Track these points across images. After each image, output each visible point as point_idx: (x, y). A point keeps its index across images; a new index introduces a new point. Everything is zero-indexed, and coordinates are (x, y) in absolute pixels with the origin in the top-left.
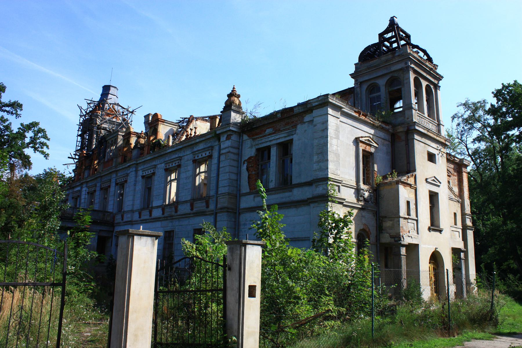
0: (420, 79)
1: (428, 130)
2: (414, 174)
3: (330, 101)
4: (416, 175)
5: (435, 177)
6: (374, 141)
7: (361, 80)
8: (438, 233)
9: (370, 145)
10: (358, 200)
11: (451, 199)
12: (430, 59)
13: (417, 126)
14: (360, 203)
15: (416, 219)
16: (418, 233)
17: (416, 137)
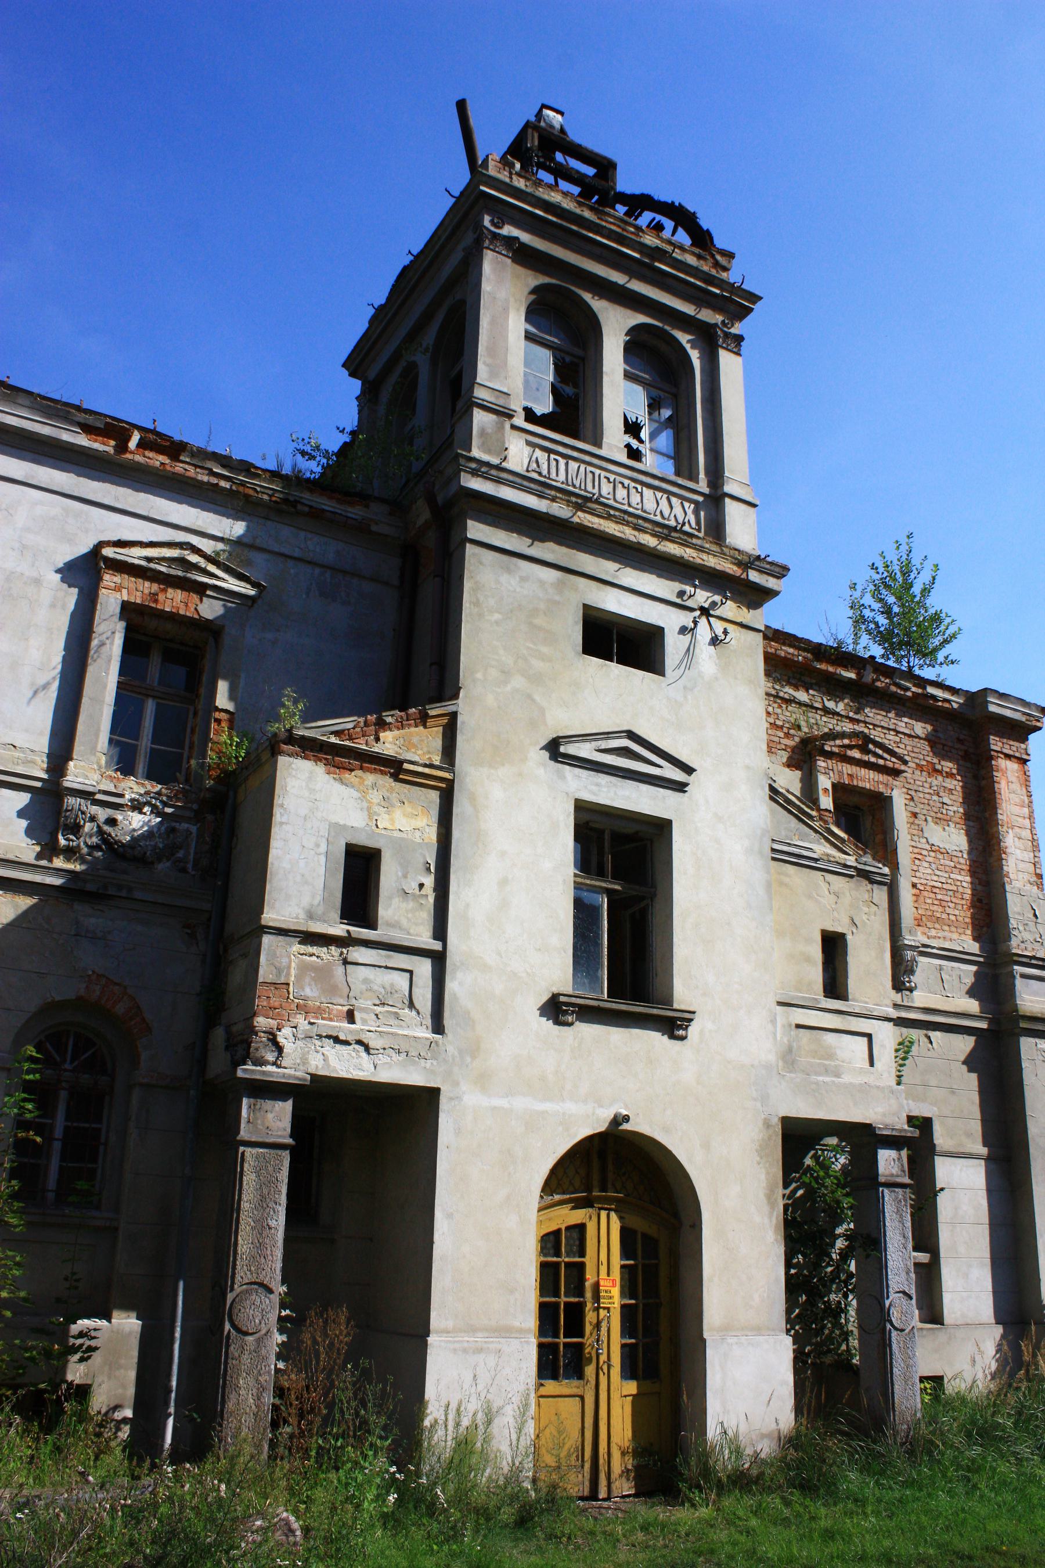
0: (587, 297)
1: (666, 532)
2: (450, 707)
3: (992, 708)
4: (453, 716)
5: (631, 735)
6: (228, 570)
7: (372, 374)
8: (656, 1039)
9: (201, 589)
10: (50, 849)
11: (785, 856)
12: (702, 239)
13: (475, 473)
14: (59, 863)
15: (437, 946)
16: (438, 1028)
17: (476, 529)
